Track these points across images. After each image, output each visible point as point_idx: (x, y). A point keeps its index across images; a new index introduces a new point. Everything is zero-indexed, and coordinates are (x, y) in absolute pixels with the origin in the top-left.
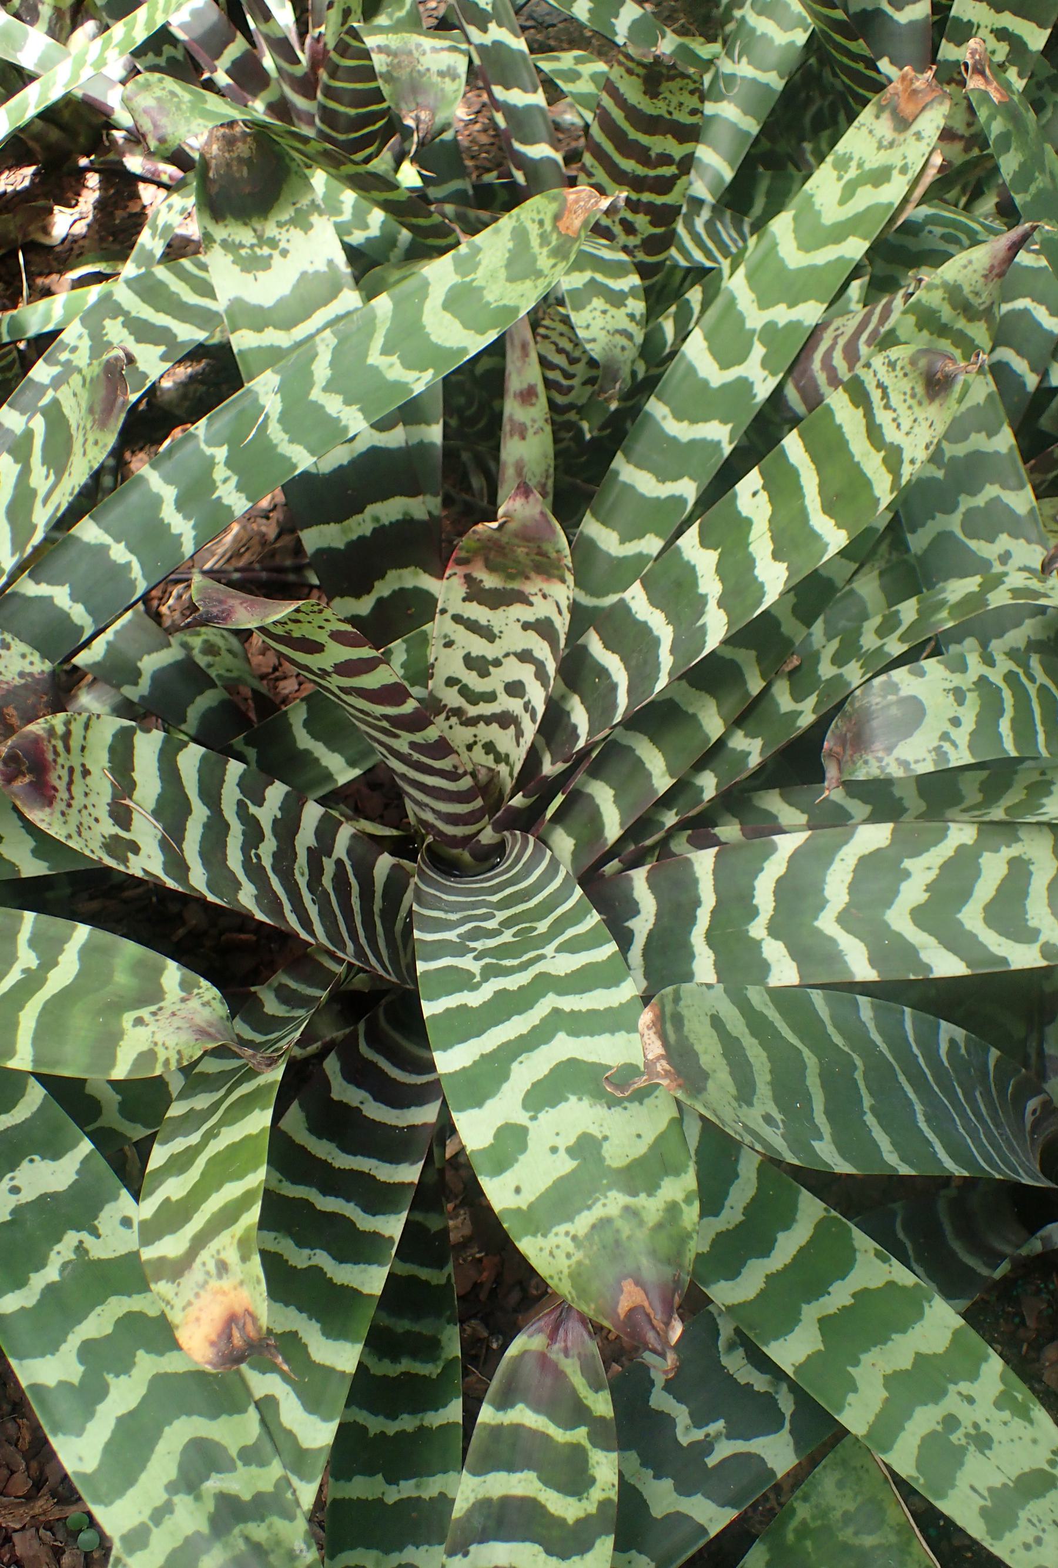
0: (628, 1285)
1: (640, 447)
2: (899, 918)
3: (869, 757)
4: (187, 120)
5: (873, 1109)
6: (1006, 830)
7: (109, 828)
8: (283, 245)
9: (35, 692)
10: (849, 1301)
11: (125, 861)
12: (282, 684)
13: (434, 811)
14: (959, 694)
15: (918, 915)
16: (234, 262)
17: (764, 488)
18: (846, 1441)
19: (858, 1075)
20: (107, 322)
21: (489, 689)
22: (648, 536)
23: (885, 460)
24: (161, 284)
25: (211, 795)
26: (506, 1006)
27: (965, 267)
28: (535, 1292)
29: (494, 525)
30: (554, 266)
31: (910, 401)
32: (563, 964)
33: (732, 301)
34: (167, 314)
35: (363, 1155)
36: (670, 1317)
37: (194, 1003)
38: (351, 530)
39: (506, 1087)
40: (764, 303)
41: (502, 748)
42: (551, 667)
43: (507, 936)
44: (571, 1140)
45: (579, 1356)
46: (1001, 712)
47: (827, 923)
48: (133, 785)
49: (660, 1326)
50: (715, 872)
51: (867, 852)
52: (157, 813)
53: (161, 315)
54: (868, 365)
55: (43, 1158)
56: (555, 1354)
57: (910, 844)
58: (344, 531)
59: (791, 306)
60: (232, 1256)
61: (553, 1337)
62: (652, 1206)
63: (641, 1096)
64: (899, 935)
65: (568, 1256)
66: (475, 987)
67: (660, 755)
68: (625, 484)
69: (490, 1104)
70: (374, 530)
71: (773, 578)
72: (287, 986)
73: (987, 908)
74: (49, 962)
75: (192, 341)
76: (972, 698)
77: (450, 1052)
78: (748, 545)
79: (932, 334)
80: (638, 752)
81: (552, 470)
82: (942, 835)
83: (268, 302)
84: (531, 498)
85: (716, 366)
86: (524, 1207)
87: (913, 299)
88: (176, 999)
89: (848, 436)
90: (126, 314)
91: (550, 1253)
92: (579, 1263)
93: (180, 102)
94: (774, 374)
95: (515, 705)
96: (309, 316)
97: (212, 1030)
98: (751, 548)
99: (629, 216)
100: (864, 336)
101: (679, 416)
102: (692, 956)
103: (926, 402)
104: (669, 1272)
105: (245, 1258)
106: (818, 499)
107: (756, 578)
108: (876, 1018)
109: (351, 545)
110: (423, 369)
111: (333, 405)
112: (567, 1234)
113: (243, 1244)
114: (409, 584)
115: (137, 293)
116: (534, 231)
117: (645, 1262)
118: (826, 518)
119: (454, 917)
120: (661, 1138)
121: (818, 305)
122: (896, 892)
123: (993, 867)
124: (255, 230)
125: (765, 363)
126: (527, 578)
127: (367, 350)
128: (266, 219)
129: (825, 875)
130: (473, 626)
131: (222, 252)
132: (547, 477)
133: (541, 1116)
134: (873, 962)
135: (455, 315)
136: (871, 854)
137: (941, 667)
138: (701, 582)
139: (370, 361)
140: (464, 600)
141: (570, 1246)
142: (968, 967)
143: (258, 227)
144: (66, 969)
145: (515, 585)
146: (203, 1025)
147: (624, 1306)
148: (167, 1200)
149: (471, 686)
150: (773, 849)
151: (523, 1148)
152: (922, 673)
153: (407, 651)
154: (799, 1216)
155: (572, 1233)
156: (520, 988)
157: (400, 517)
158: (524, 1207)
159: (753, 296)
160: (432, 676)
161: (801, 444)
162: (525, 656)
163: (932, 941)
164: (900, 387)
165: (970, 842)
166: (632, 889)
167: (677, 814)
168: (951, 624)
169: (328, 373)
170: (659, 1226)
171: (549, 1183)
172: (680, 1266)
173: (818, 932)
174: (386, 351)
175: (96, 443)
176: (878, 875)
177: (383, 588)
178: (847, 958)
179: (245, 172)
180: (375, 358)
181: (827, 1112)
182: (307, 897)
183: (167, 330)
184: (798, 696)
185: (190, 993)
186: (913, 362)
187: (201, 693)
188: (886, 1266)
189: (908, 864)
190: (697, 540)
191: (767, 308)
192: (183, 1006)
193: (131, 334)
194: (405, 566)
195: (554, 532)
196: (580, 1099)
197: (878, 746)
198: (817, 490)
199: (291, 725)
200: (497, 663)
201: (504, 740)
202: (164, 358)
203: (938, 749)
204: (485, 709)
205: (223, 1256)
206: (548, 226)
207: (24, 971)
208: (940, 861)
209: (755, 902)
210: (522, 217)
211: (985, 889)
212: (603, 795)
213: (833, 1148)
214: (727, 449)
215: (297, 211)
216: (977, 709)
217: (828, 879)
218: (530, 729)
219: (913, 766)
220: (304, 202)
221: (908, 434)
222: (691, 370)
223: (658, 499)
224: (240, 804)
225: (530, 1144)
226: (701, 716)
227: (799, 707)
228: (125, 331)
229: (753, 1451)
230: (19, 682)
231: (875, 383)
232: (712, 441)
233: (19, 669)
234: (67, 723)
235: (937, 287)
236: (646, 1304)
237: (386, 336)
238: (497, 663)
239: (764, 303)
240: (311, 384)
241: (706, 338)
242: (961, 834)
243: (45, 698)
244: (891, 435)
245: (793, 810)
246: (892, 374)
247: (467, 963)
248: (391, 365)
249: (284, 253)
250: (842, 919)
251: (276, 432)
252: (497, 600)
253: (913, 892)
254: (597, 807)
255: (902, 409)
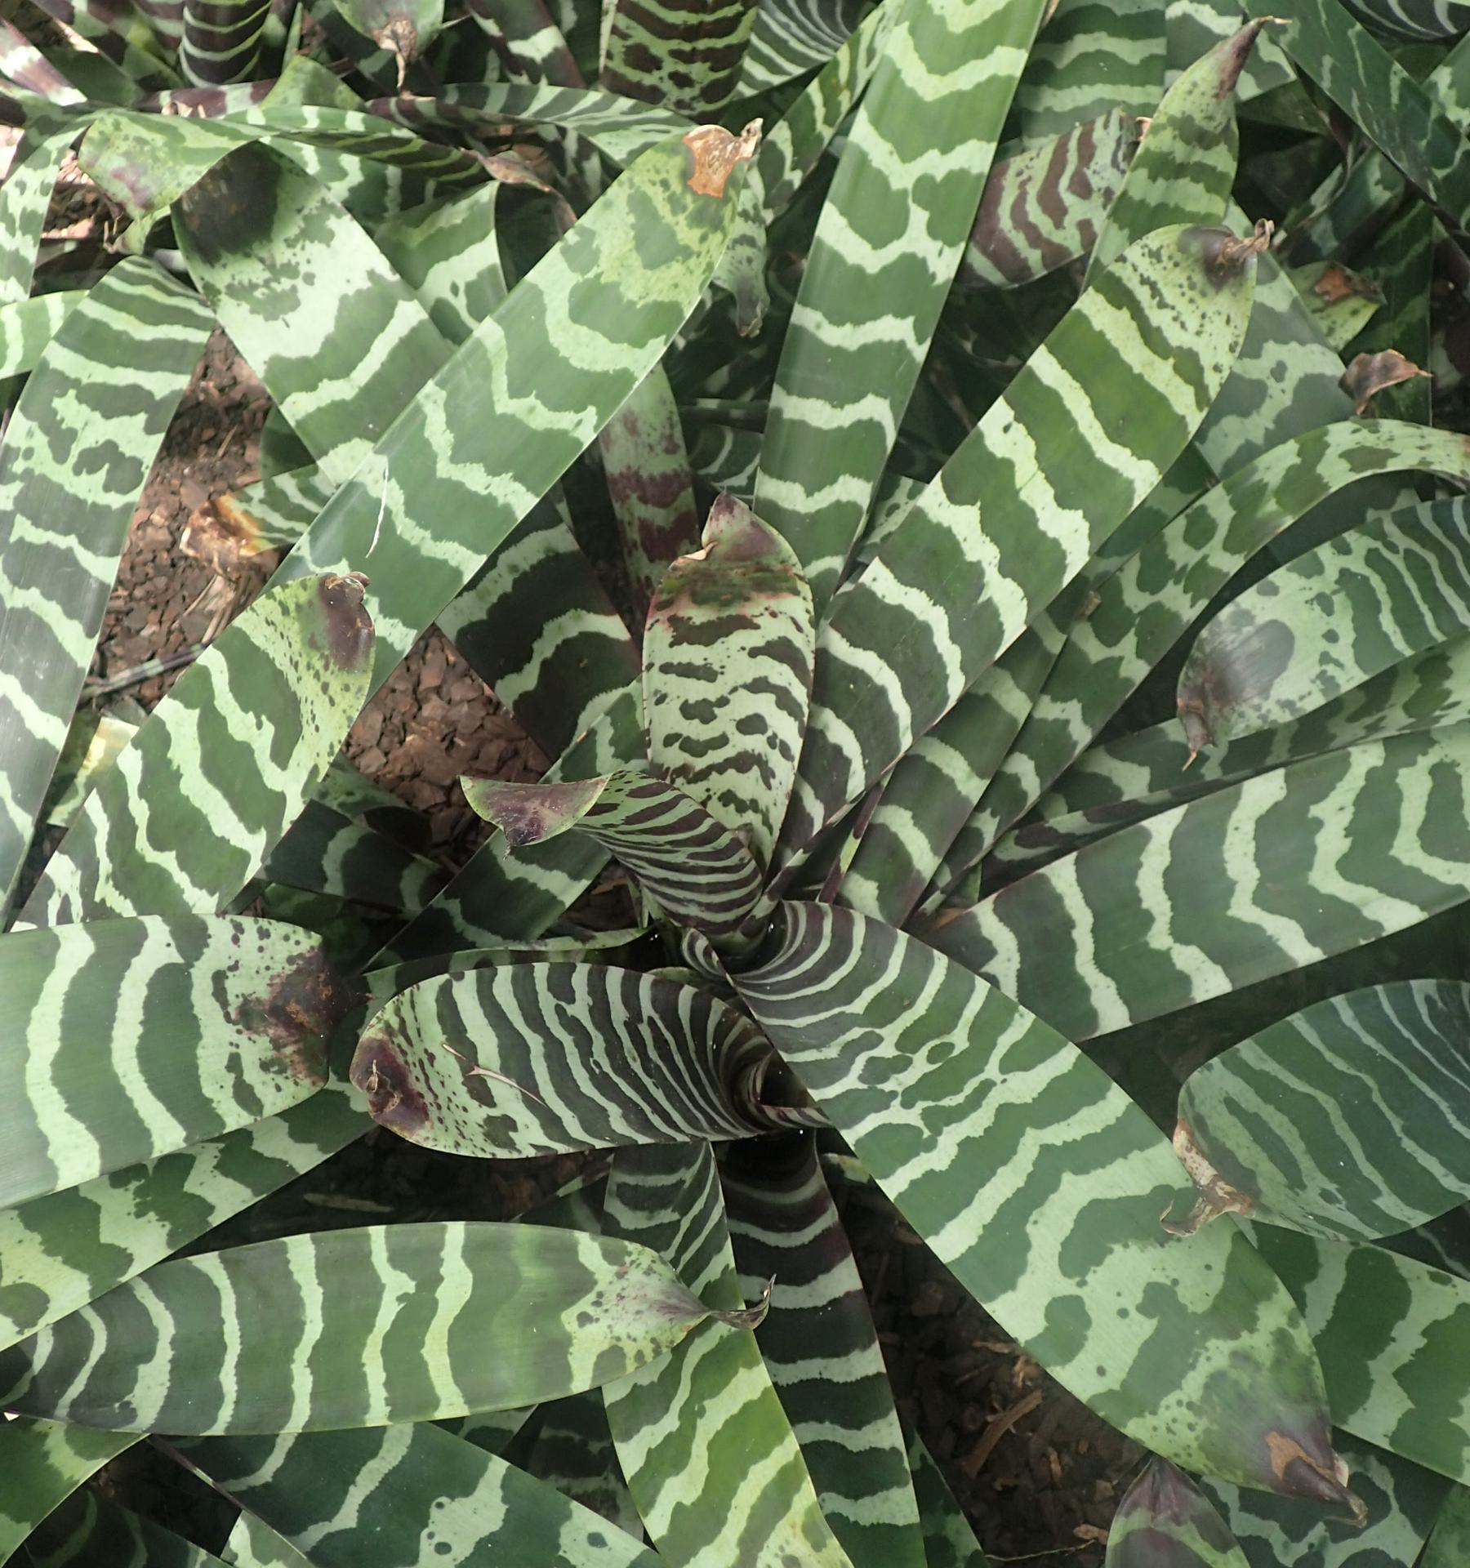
0: (1274, 1440)
1: (799, 372)
2: (1326, 879)
3: (1244, 708)
4: (173, 171)
5: (1407, 1131)
6: (1417, 739)
7: (479, 1113)
8: (304, 269)
9: (310, 974)
10: (1421, 1342)
11: (511, 1145)
12: (363, 762)
13: (700, 904)
14: (1324, 602)
15: (1347, 867)
16: (252, 311)
17: (1017, 419)
18: (1454, 1493)
19: (1376, 1097)
20: (57, 403)
21: (717, 734)
22: (841, 479)
23: (1177, 369)
24: (97, 324)
25: (536, 1021)
26: (981, 1159)
27: (1190, 92)
28: (972, 1427)
29: (700, 555)
30: (703, 239)
31: (1190, 294)
32: (1024, 1087)
33: (863, 160)
34: (127, 366)
35: (803, 1358)
36: (1332, 1459)
37: (635, 1275)
38: (488, 593)
39: (1032, 1256)
40: (907, 154)
41: (744, 794)
42: (800, 693)
43: (920, 1065)
44: (1139, 1297)
45: (1193, 1519)
46: (1376, 607)
47: (1243, 908)
48: (473, 1046)
49: (1326, 1473)
50: (1080, 881)
51: (1263, 811)
52: (505, 1070)
53: (120, 370)
54: (1122, 259)
55: (453, 1498)
56: (1163, 1523)
57: (1309, 788)
58: (481, 597)
59: (945, 150)
60: (800, 1547)
61: (1154, 1506)
62: (1259, 1342)
63: (1184, 1222)
64: (1333, 899)
65: (1191, 1427)
66: (930, 1146)
67: (957, 754)
68: (793, 422)
69: (1023, 1282)
70: (515, 582)
71: (1071, 534)
72: (625, 1184)
73: (1422, 833)
74: (429, 1281)
75: (174, 393)
76: (1340, 601)
77: (943, 1233)
78: (1017, 492)
79: (1167, 179)
80: (929, 758)
81: (676, 418)
82: (1345, 764)
83: (312, 349)
84: (736, 511)
85: (867, 246)
86: (1117, 1387)
87: (1140, 151)
88: (610, 1277)
89: (1115, 343)
90: (76, 383)
91: (1167, 1427)
92: (1207, 1431)
93: (154, 150)
94: (952, 244)
95: (755, 743)
96: (366, 350)
97: (673, 1301)
98: (1023, 496)
99: (682, 68)
100: (1064, 182)
101: (837, 320)
102: (1086, 991)
103: (1211, 291)
104: (1309, 1409)
105: (818, 1546)
106: (1097, 425)
107: (1043, 534)
108: (1358, 1015)
109: (494, 610)
110: (580, 408)
111: (475, 478)
112: (1179, 1403)
113: (809, 1530)
114: (573, 632)
115: (76, 349)
116: (658, 196)
117: (1280, 1407)
118: (1117, 447)
119: (832, 1052)
120: (1231, 1260)
121: (984, 144)
122: (1312, 849)
123: (1415, 784)
124: (262, 260)
125: (933, 231)
126: (747, 599)
127: (490, 396)
128: (270, 240)
129: (1221, 852)
130: (687, 671)
131: (233, 302)
132: (672, 426)
133: (1089, 1278)
134: (1312, 939)
135: (593, 327)
136: (1269, 812)
137: (1295, 576)
138: (965, 546)
139: (500, 409)
140: (671, 645)
141: (1190, 1417)
142: (1423, 909)
143: (264, 254)
144: (456, 1285)
145: (733, 611)
146: (661, 1297)
147: (1278, 1464)
148: (679, 1508)
149: (694, 736)
150: (1146, 836)
151: (1086, 1322)
152: (1274, 590)
153: (613, 724)
154: (1322, 1259)
155: (1185, 1400)
156: (986, 1130)
157: (542, 556)
158: (1117, 1387)
159: (889, 146)
160: (649, 744)
161: (1054, 360)
162: (759, 686)
163: (1371, 892)
164: (1171, 280)
165: (1380, 763)
166: (978, 926)
167: (993, 815)
168: (1289, 521)
169: (449, 437)
170: (1278, 1363)
171: (1134, 1352)
172: (1316, 1399)
173: (1237, 923)
174: (516, 392)
175: (347, 688)
176: (1284, 834)
177: (544, 649)
178: (1281, 943)
179: (224, 189)
180: (505, 404)
181: (1369, 1159)
182: (648, 1082)
183: (135, 389)
184: (1109, 637)
185: (623, 1264)
186: (1182, 248)
187: (332, 836)
188: (1448, 1289)
189: (1315, 811)
190: (943, 496)
191: (914, 158)
192: (623, 1283)
193: (94, 409)
194: (563, 612)
195: (772, 541)
196: (1126, 1246)
197: (1249, 692)
198: (1091, 413)
199: (495, 858)
200: (723, 702)
201: (747, 785)
202: (150, 429)
203: (1322, 676)
204: (716, 757)
205: (789, 1551)
206: (676, 186)
207: (400, 1299)
208: (1352, 796)
209: (1145, 905)
210: (637, 180)
211: (1413, 812)
212: (899, 821)
213: (1394, 1198)
214: (920, 352)
215: (306, 219)
216: (1350, 613)
217: (1227, 856)
218: (785, 772)
219: (1299, 705)
220: (312, 205)
221: (1198, 333)
222: (836, 258)
223: (840, 429)
224: (560, 1011)
225: (1092, 1314)
226: (996, 695)
227: (1115, 652)
228: (84, 408)
229: (1368, 1546)
230: (290, 969)
231: (1137, 279)
232: (891, 343)
233: (286, 955)
234: (397, 1012)
235: (1164, 127)
236: (1302, 1454)
237: (508, 373)
238: (723, 702)
239: (907, 154)
240: (433, 458)
241: (843, 213)
242: (1366, 758)
243: (323, 977)
244: (1175, 337)
245: (1127, 765)
246: (1159, 266)
247: (896, 1114)
248: (531, 410)
249: (310, 279)
250: (1261, 899)
251: (408, 530)
252: (709, 634)
253: (1332, 842)
254: (895, 836)
255: (1182, 305)
